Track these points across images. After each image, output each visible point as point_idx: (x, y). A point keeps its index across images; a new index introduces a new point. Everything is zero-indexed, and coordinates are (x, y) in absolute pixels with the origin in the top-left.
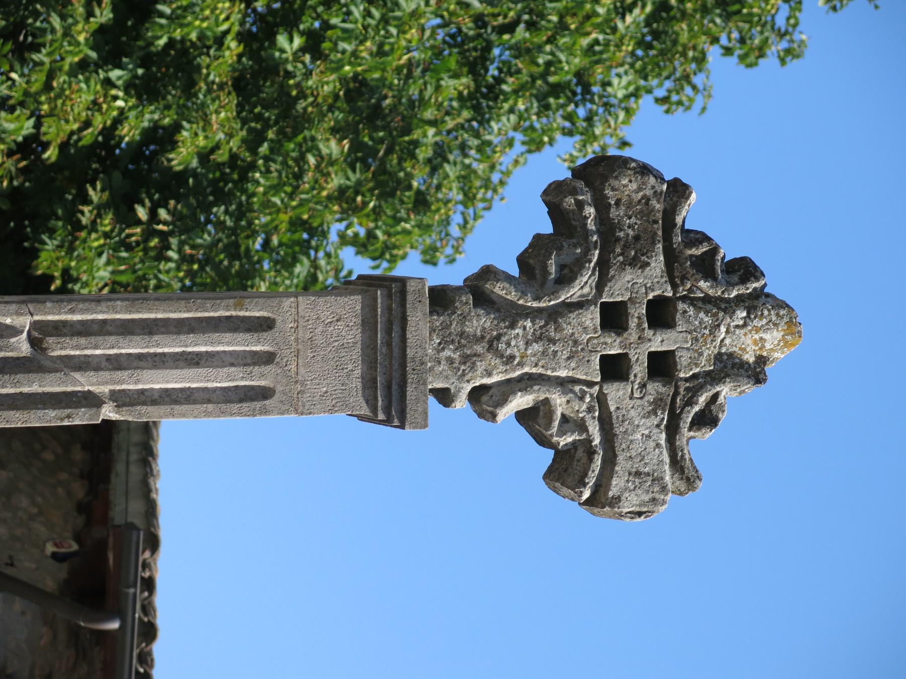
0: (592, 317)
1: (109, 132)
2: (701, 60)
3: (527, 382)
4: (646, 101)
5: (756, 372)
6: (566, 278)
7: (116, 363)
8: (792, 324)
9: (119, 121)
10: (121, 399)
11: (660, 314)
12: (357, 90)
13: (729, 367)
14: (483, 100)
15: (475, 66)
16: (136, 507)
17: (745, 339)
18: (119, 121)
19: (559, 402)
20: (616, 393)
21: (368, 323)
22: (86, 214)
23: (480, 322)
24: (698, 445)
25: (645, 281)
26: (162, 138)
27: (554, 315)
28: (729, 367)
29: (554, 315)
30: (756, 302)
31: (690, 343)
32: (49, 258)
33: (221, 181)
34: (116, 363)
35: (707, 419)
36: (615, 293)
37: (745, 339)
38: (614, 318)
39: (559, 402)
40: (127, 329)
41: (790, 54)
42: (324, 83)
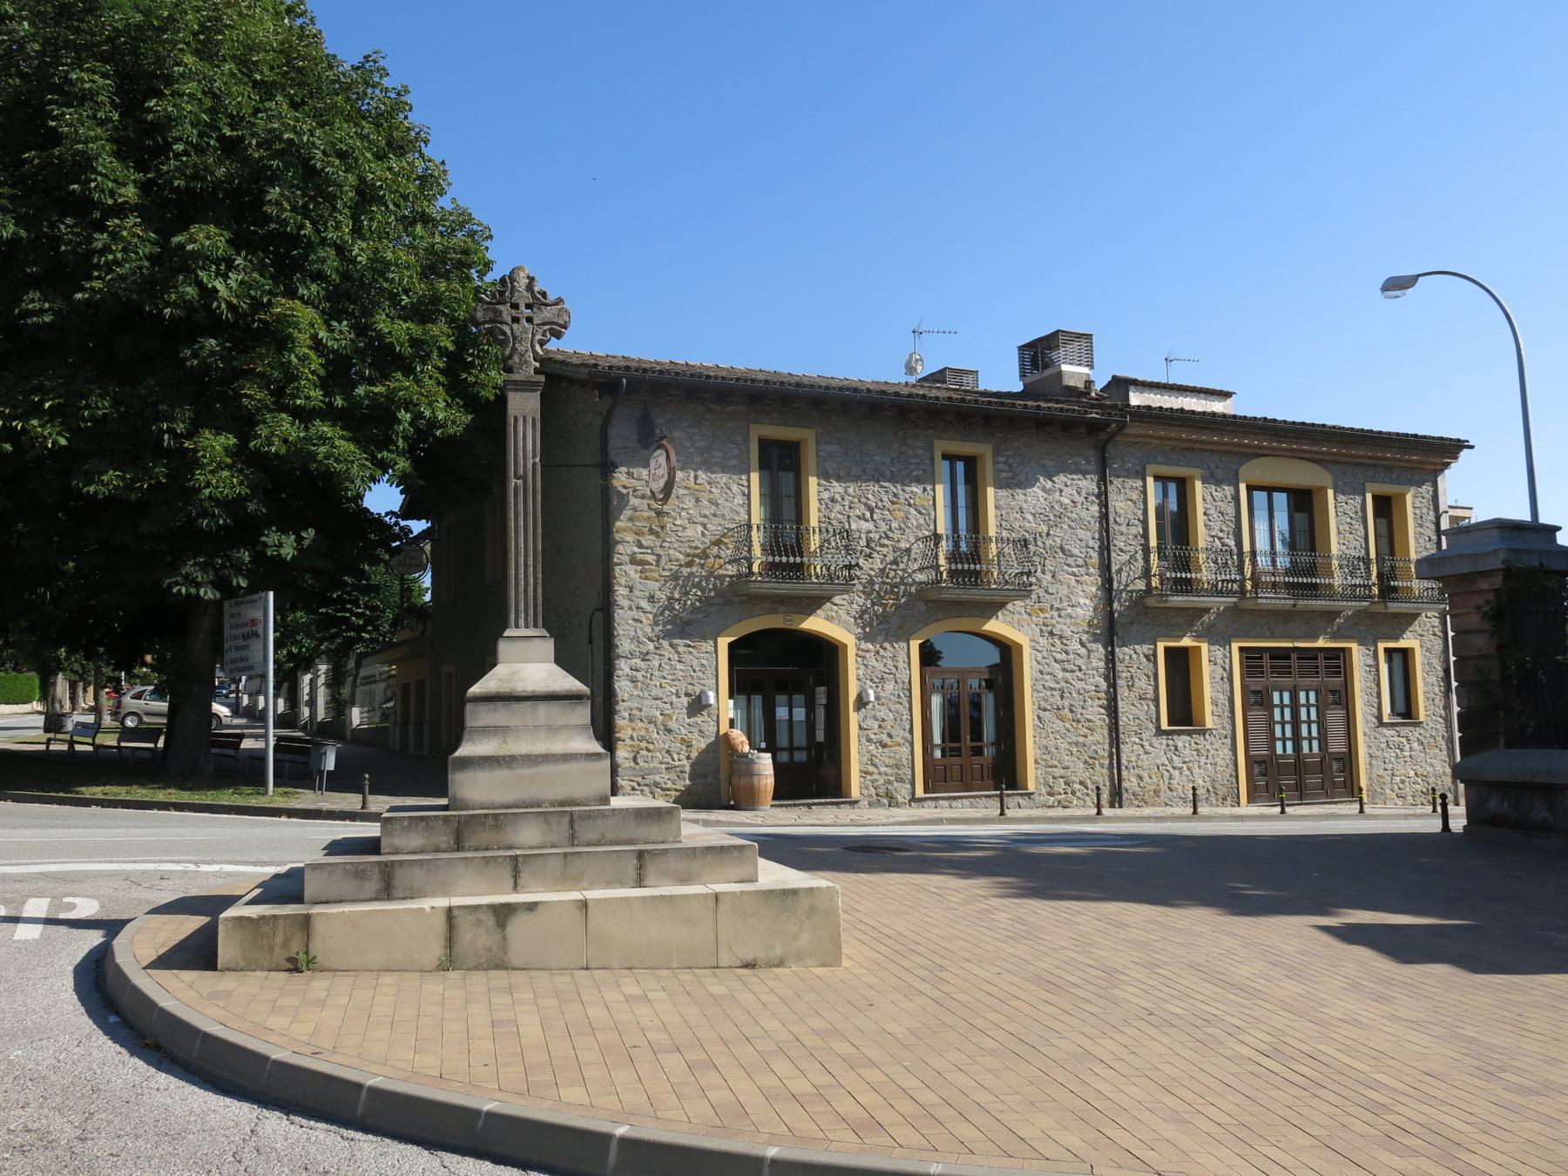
0: (515, 326)
1: (441, 371)
2: (409, 129)
3: (533, 346)
4: (424, 150)
5: (531, 279)
6: (504, 334)
7: (525, 457)
8: (519, 268)
9: (437, 368)
10: (534, 456)
11: (515, 306)
12: (424, 275)
13: (530, 288)
14: (426, 219)
15: (413, 223)
16: (583, 370)
17: (522, 282)
18: (437, 368)
19: (538, 337)
20: (536, 321)
21: (516, 390)
22: (471, 379)
23: (516, 358)
24: (551, 297)
25: (506, 312)
26: (443, 352)
27: (514, 338)
28: (530, 288)
29: (514, 338)
30: (512, 280)
31: (523, 298)
32: (489, 394)
33: (461, 330)
34: (525, 457)
35: (544, 294)
36: (509, 320)
37: (522, 282)
38: (516, 320)
39: (538, 337)
40: (516, 455)
41: (407, 92)
42: (420, 288)
